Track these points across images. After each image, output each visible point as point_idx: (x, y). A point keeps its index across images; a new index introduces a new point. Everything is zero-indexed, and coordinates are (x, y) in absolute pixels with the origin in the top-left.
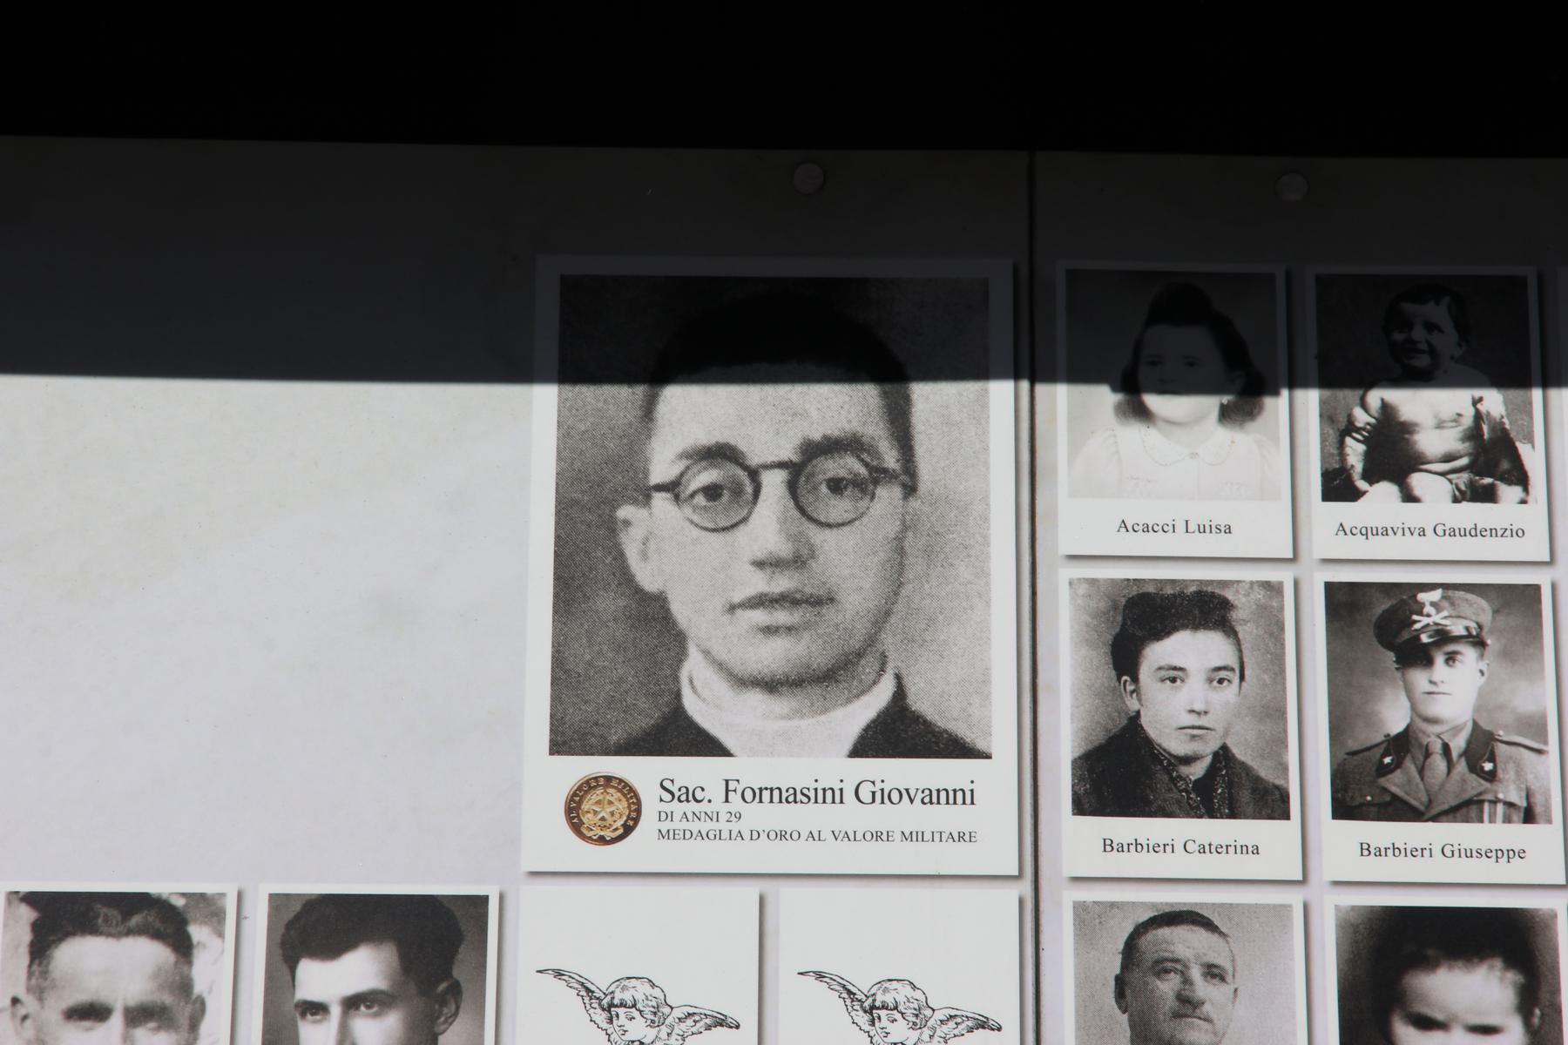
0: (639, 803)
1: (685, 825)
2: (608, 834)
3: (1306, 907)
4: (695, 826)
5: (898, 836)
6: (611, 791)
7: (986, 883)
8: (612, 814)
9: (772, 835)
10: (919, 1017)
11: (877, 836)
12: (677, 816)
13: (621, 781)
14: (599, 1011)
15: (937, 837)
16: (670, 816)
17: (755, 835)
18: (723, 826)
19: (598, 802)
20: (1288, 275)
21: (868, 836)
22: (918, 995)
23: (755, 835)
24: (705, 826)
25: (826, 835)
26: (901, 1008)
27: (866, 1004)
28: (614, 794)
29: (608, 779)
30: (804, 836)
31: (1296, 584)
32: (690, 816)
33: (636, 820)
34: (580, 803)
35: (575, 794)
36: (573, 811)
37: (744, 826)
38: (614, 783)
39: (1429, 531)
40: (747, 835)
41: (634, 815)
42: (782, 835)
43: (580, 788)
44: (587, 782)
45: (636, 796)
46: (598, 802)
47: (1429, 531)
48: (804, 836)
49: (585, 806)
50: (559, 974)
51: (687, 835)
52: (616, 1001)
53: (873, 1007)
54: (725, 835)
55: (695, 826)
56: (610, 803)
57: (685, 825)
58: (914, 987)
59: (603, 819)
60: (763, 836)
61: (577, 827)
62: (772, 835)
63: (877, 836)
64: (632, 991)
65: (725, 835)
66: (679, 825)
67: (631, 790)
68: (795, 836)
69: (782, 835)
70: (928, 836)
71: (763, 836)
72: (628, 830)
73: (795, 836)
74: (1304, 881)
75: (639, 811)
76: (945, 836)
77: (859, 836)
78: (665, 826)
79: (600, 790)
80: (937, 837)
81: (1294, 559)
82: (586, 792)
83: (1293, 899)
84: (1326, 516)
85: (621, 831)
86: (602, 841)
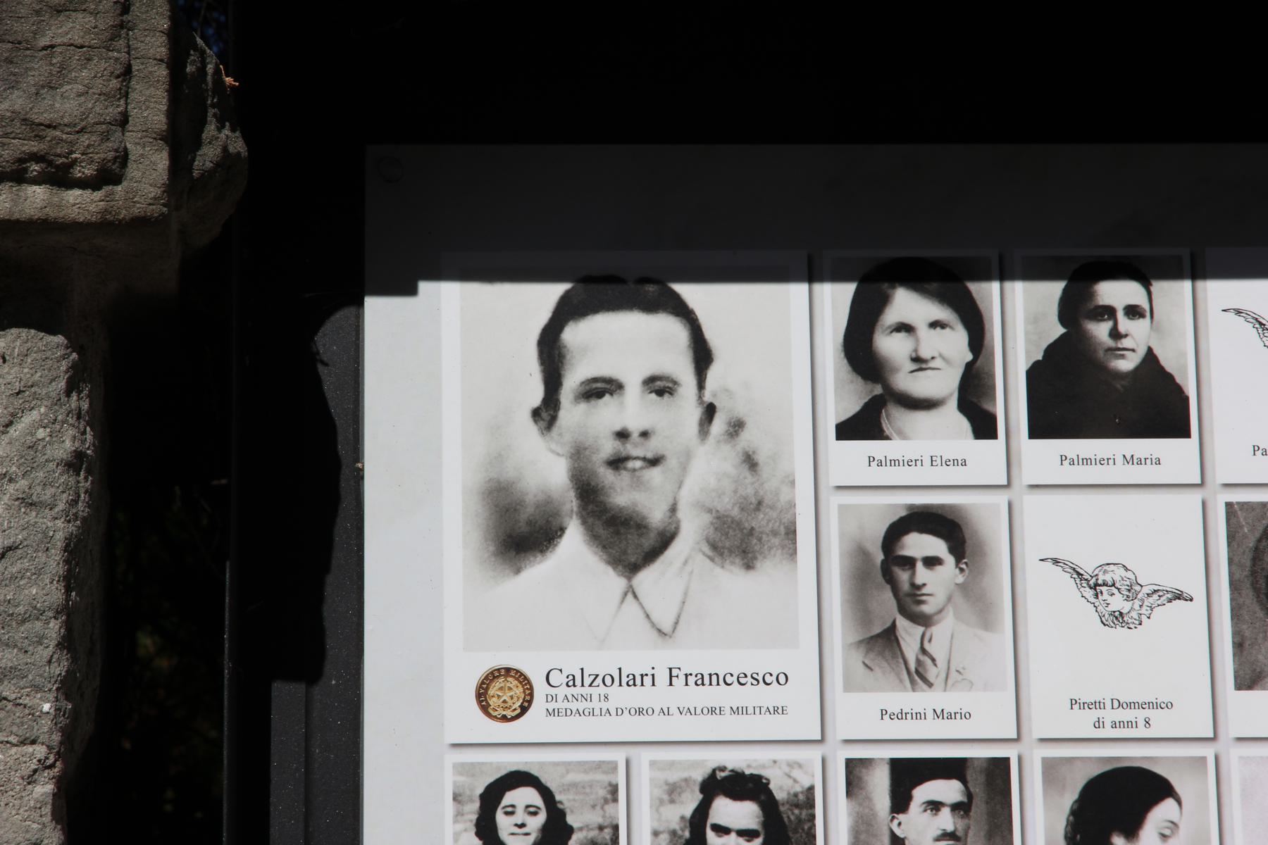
0: (531, 689)
1: (566, 705)
2: (509, 714)
4: (574, 706)
5: (728, 710)
6: (510, 679)
8: (512, 697)
9: (633, 712)
11: (712, 711)
13: (518, 671)
15: (757, 710)
16: (554, 698)
17: (620, 712)
18: (596, 704)
19: (501, 689)
21: (705, 711)
23: (620, 712)
24: (581, 705)
25: (674, 710)
28: (512, 682)
30: (657, 712)
32: (570, 697)
33: (530, 702)
34: (487, 689)
35: (483, 683)
38: (512, 673)
40: (613, 712)
41: (528, 698)
42: (640, 711)
43: (486, 678)
44: (492, 673)
45: (529, 683)
46: (501, 689)
48: (657, 712)
49: (491, 692)
51: (568, 713)
54: (597, 712)
55: (574, 706)
56: (510, 689)
57: (566, 705)
59: (505, 702)
60: (626, 712)
61: (485, 709)
62: (633, 712)
63: (712, 711)
66: (561, 705)
67: (526, 678)
68: (650, 711)
69: (640, 711)
70: (750, 710)
71: (626, 712)
73: (650, 711)
75: (531, 695)
76: (763, 710)
77: (699, 711)
78: (551, 706)
80: (757, 710)
86: (504, 719)
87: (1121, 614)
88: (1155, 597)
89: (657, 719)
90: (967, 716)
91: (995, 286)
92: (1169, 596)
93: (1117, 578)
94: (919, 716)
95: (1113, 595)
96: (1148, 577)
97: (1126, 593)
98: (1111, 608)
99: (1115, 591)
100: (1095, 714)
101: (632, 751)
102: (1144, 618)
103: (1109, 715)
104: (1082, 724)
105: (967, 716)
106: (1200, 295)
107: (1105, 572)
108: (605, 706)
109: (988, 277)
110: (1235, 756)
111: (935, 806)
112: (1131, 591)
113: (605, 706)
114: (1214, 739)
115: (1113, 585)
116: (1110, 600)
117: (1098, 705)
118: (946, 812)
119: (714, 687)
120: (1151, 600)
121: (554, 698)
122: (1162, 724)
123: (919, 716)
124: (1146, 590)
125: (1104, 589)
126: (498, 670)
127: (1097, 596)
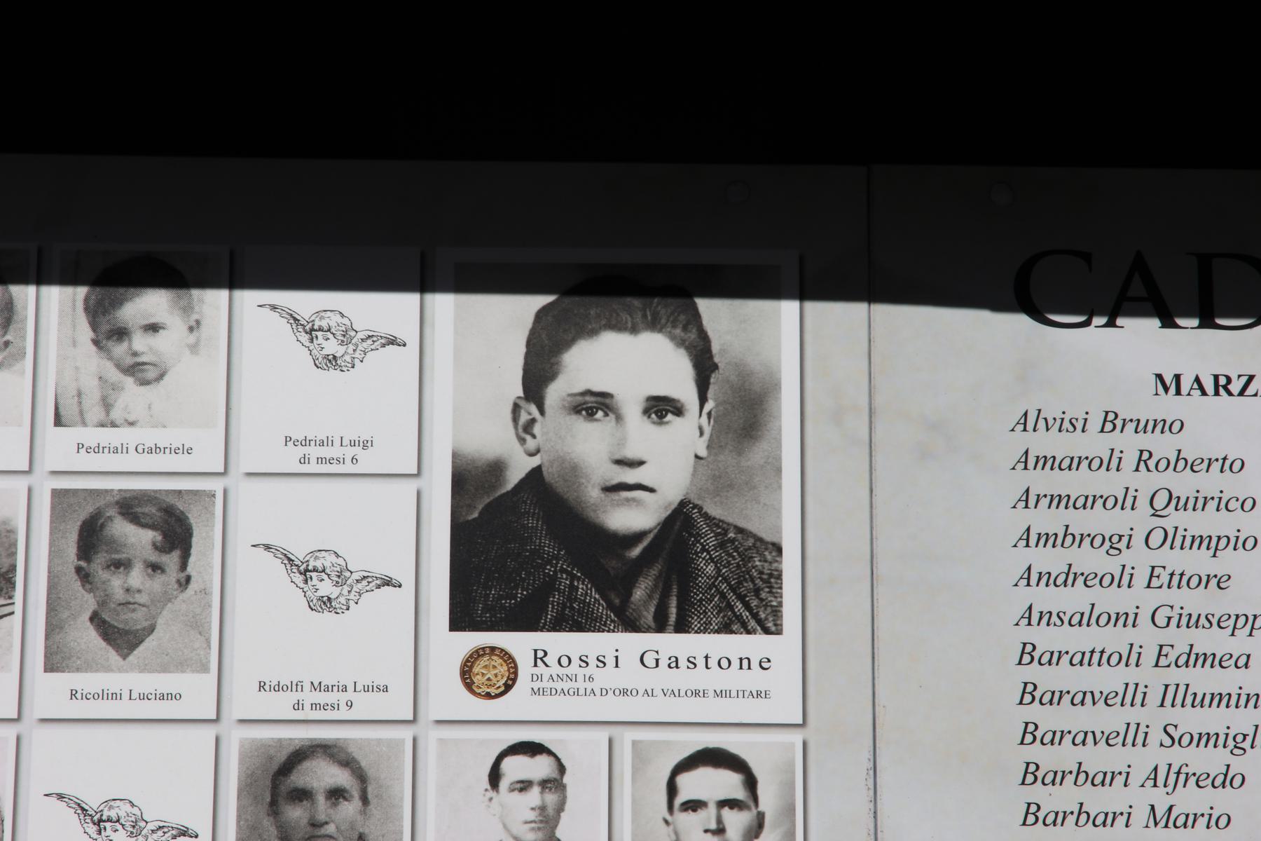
0: (516, 667)
1: (551, 684)
2: (493, 691)
3: (415, 740)
4: (559, 685)
5: (711, 693)
6: (495, 658)
7: (147, 726)
8: (496, 675)
9: (617, 692)
10: (135, 828)
11: (696, 693)
12: (545, 678)
13: (502, 650)
14: (91, 825)
15: (741, 694)
16: (540, 678)
17: (604, 692)
18: (581, 684)
19: (486, 667)
20: (40, 251)
21: (689, 693)
22: (135, 811)
23: (604, 692)
24: (566, 685)
25: (658, 692)
26: (122, 821)
27: (95, 818)
28: (497, 661)
29: (493, 649)
30: (641, 693)
31: (225, 492)
32: (555, 677)
33: (514, 680)
34: (471, 667)
35: (467, 661)
36: (466, 673)
37: (596, 686)
38: (497, 652)
39: (132, 450)
40: (598, 692)
41: (512, 676)
42: (624, 692)
43: (471, 656)
44: (477, 651)
45: (514, 661)
46: (486, 667)
47: (132, 450)
48: (641, 693)
49: (476, 669)
50: (60, 797)
51: (553, 692)
52: (104, 818)
53: (100, 821)
54: (582, 692)
55: (559, 685)
56: (494, 667)
57: (551, 684)
58: (133, 805)
59: (489, 679)
60: (610, 693)
61: (469, 686)
62: (617, 692)
63: (696, 693)
64: (117, 810)
65: (582, 692)
66: (546, 684)
67: (510, 657)
68: (634, 693)
69: (624, 692)
70: (734, 694)
71: (610, 693)
72: (508, 688)
73: (634, 693)
74: (803, 725)
75: (516, 673)
76: (746, 694)
77: (682, 693)
78: (536, 685)
79: (486, 658)
80: (741, 694)
81: (29, 472)
82: (476, 659)
83: (406, 734)
84: (52, 437)
85: (503, 689)
86: (488, 696)
87: (329, 599)
88: (365, 583)
89: (641, 700)
90: (177, 697)
91: (31, 290)
92: (378, 582)
93: (327, 564)
94: (115, 696)
95: (323, 582)
96: (357, 565)
97: (336, 579)
98: (319, 594)
99: (325, 577)
100: (293, 697)
101: (615, 731)
102: (352, 603)
103: (309, 697)
104: (280, 706)
105: (177, 697)
106: (43, 302)
107: (316, 558)
108: (589, 686)
109: (24, 280)
110: (432, 738)
111: (524, 786)
112: (341, 578)
113: (589, 686)
114: (414, 721)
115: (324, 571)
116: (319, 585)
117: (297, 686)
118: (536, 790)
119: (745, 671)
120: (359, 586)
121: (540, 678)
122: (366, 706)
123: (115, 696)
124: (356, 576)
125: (314, 575)
126: (483, 649)
127: (306, 582)
